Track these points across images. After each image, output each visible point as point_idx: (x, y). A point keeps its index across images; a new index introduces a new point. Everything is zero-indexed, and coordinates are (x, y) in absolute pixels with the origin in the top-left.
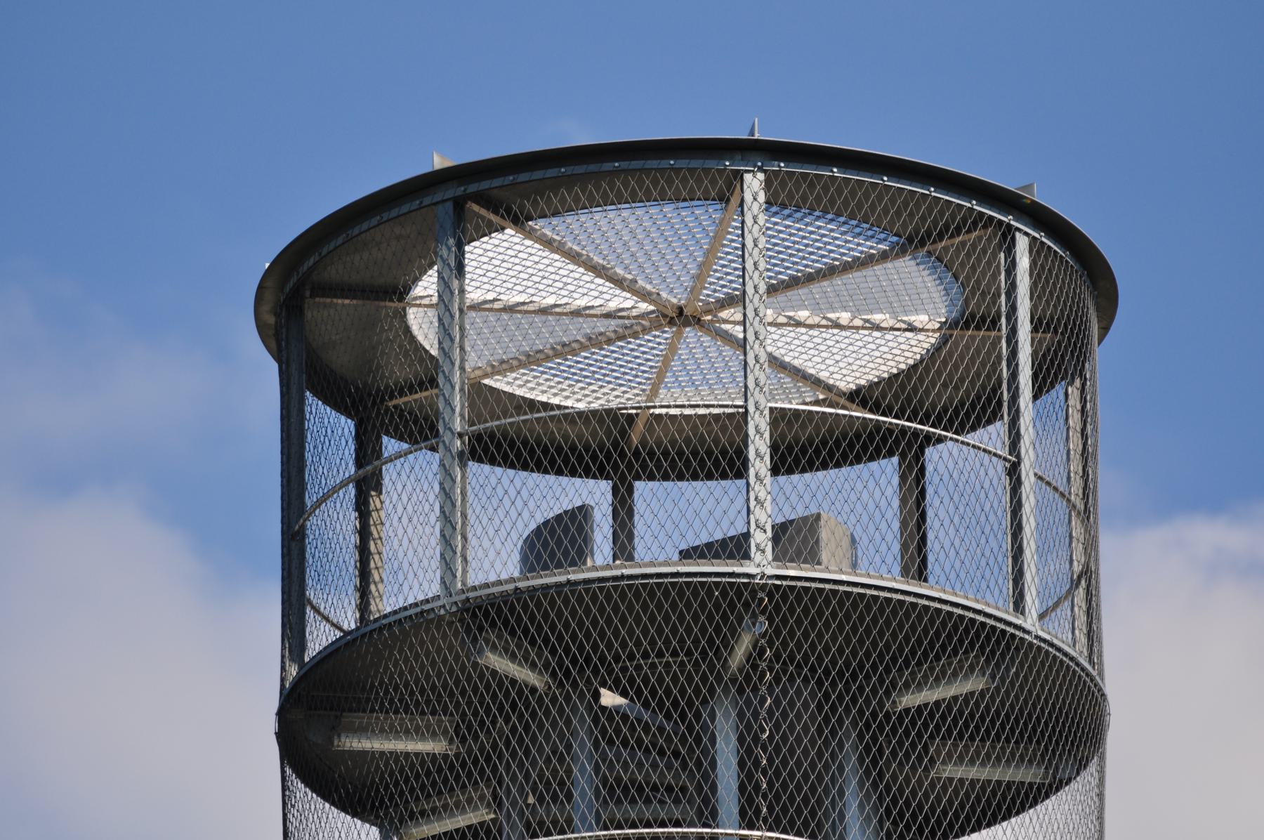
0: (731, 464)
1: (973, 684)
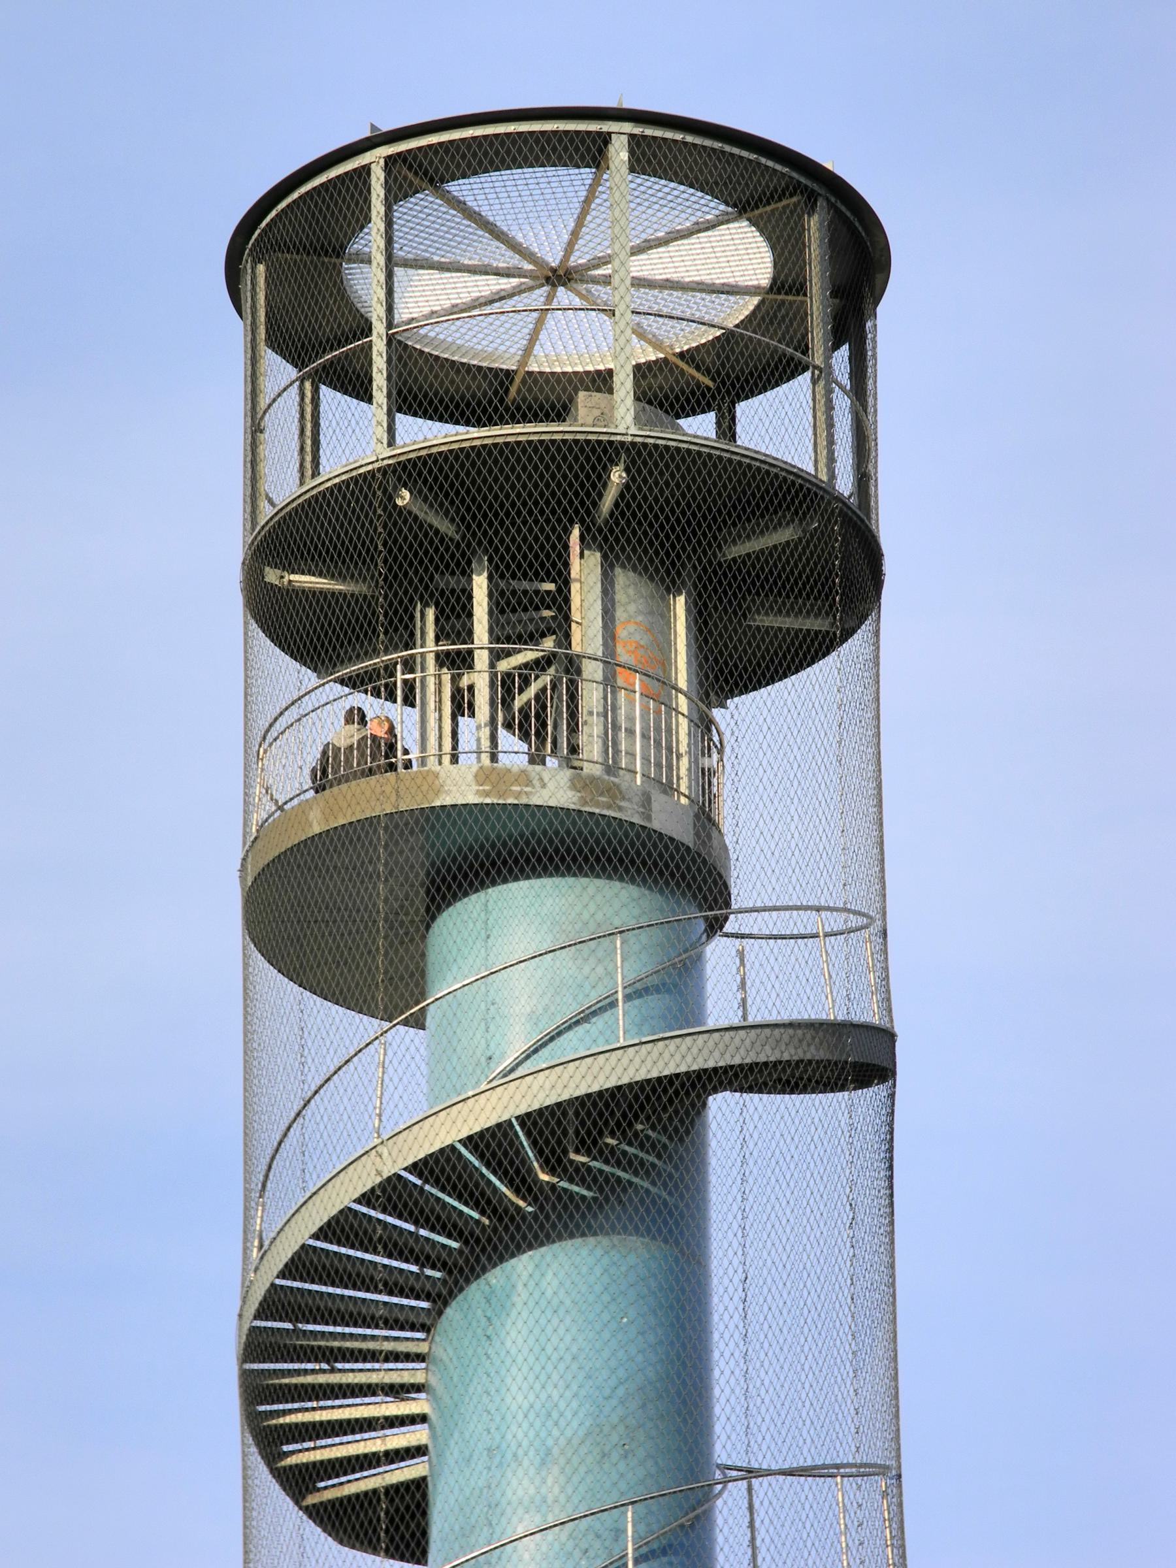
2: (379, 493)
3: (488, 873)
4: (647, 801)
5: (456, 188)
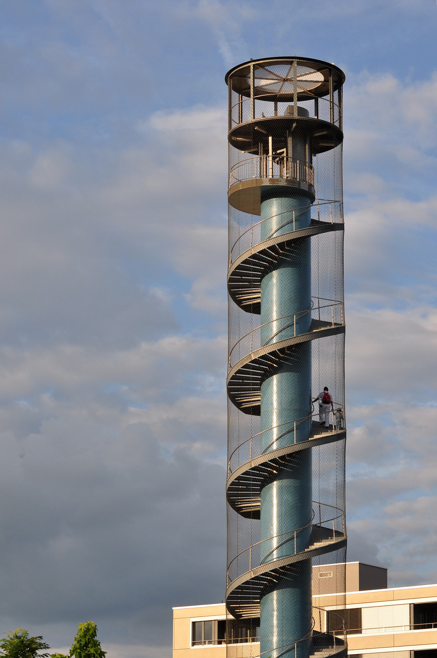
0: (291, 100)
1: (325, 133)
2: (252, 128)
3: (271, 196)
4: (299, 183)
5: (266, 68)
